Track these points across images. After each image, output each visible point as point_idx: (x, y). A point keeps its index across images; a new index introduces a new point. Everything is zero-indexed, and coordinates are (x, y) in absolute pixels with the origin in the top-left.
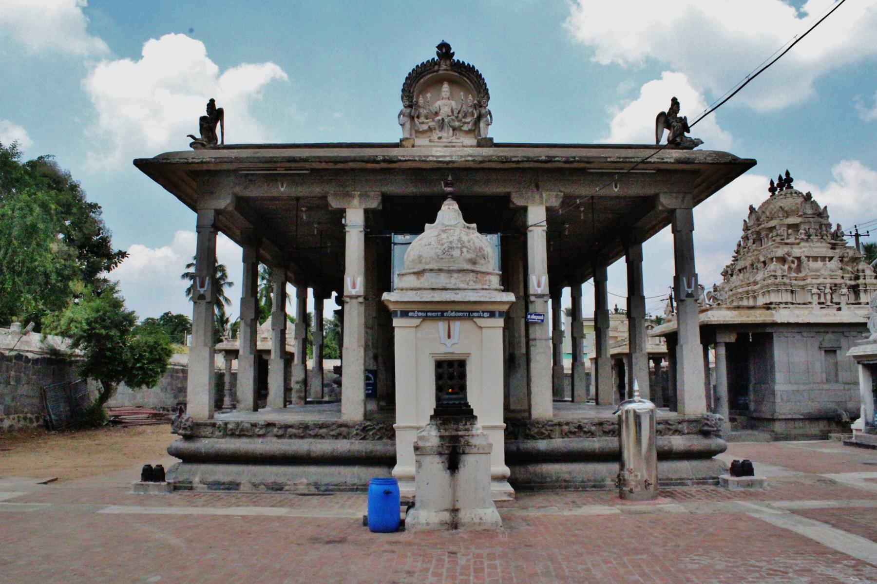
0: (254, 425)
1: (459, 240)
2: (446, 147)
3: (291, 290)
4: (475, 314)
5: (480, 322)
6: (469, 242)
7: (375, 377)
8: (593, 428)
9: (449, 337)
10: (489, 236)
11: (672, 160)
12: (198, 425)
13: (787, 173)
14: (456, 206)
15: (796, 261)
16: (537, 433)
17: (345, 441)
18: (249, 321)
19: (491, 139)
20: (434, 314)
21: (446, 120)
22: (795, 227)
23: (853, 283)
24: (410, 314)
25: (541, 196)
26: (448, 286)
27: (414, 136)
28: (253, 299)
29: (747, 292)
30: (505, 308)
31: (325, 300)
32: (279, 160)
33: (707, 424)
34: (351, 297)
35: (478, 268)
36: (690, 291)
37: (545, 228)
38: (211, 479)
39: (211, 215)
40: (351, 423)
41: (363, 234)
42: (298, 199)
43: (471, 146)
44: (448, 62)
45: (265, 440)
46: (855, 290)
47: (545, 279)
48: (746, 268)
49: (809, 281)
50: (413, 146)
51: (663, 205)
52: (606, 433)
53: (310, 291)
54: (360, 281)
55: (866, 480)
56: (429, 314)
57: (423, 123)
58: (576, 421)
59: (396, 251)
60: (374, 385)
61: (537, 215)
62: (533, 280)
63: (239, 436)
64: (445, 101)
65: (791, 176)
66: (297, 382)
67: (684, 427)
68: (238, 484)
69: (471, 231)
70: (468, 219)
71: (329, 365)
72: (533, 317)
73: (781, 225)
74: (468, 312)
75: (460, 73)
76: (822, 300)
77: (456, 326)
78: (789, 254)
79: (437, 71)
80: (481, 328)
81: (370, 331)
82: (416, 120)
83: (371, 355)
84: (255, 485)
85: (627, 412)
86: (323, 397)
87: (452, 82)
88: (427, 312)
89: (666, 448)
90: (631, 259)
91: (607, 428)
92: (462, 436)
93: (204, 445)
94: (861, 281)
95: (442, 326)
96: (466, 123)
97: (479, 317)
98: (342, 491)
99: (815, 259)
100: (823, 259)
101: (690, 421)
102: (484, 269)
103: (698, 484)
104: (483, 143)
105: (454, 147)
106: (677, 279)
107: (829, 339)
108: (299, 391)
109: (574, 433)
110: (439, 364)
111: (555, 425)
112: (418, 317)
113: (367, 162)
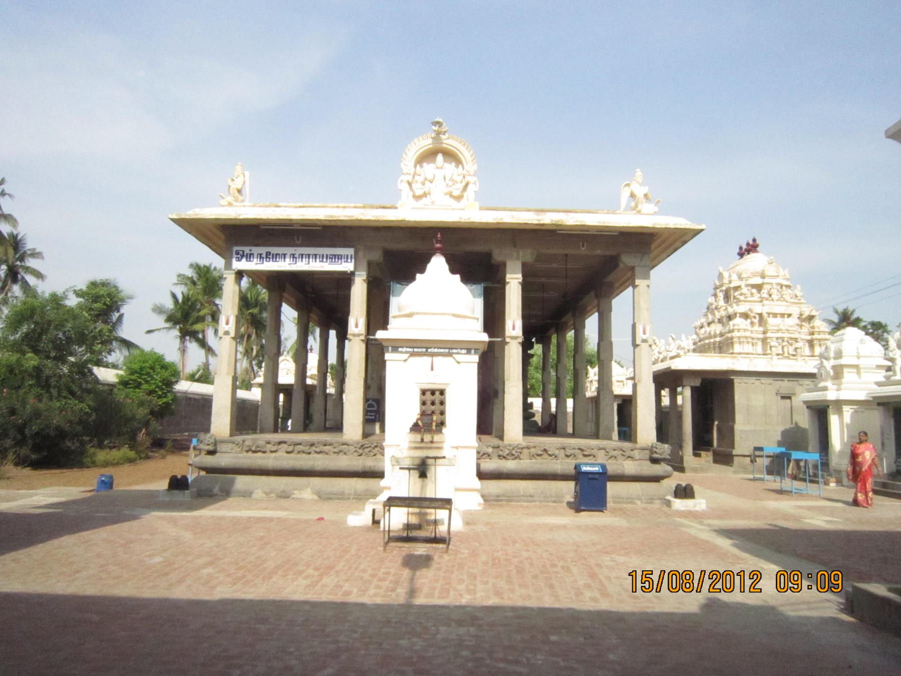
4: (454, 351)
8: (557, 452)
9: (432, 369)
10: (474, 287)
12: (222, 442)
13: (754, 240)
15: (757, 317)
17: (345, 456)
22: (759, 287)
23: (809, 338)
24: (400, 349)
28: (276, 337)
29: (714, 343)
33: (656, 452)
34: (354, 335)
36: (645, 337)
40: (351, 442)
46: (811, 343)
48: (713, 322)
49: (768, 335)
51: (624, 263)
52: (567, 456)
53: (333, 334)
55: (800, 507)
56: (416, 350)
62: (509, 324)
65: (758, 242)
67: (636, 454)
70: (453, 271)
73: (747, 285)
74: (449, 347)
76: (781, 352)
77: (438, 360)
78: (750, 310)
80: (459, 363)
94: (816, 336)
95: (427, 360)
97: (458, 353)
98: (339, 499)
99: (775, 315)
100: (782, 315)
101: (643, 449)
106: (634, 327)
107: (785, 385)
110: (424, 392)
112: (406, 352)
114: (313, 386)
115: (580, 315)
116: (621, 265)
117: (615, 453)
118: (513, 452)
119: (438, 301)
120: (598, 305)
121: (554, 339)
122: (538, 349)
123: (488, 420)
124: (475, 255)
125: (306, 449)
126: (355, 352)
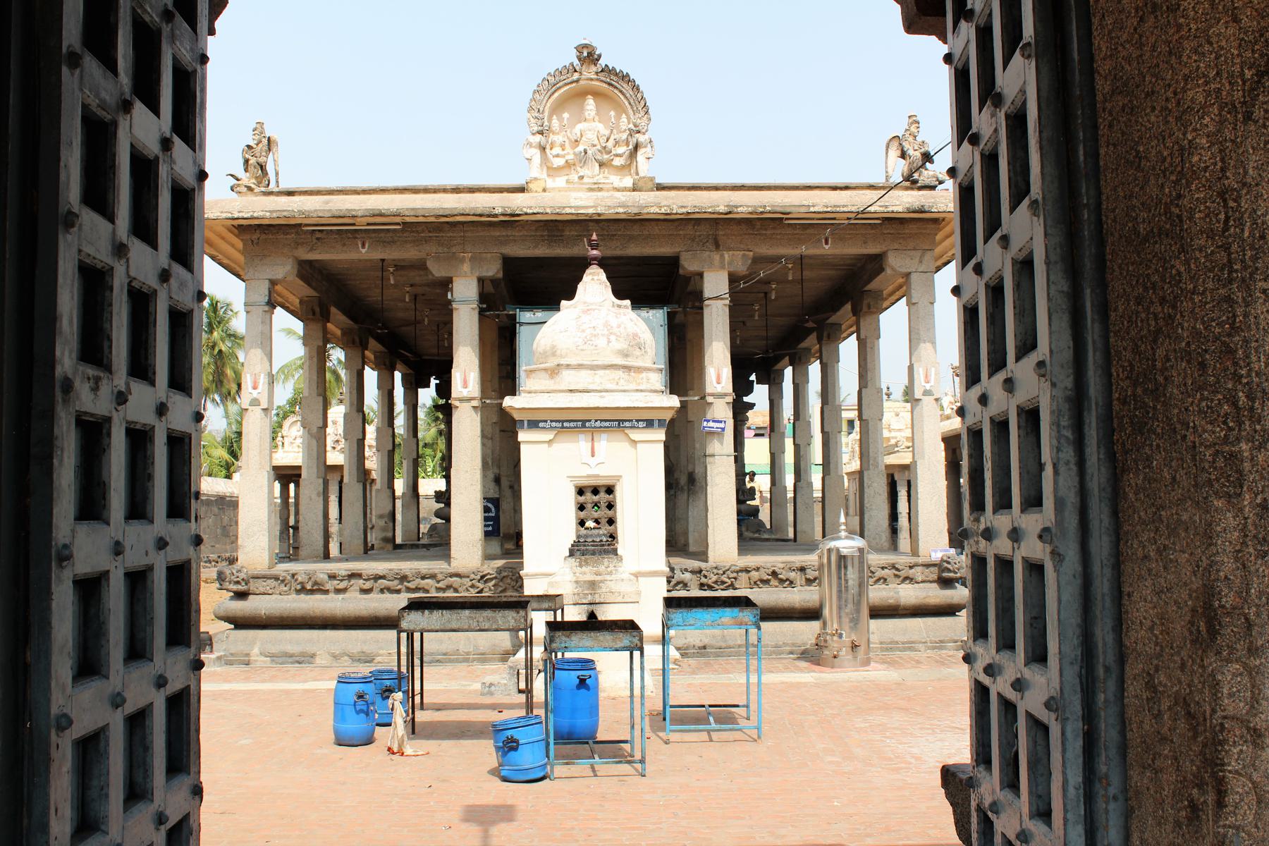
0: (332, 577)
1: (606, 324)
2: (591, 190)
3: (337, 355)
4: (627, 424)
5: (635, 435)
6: (619, 326)
7: (497, 507)
8: (792, 575)
10: (652, 312)
11: (900, 209)
14: (602, 275)
16: (716, 582)
18: (315, 430)
19: (652, 179)
20: (572, 424)
21: (589, 152)
24: (541, 425)
25: (722, 256)
26: (591, 387)
27: (544, 176)
30: (668, 416)
31: (420, 390)
32: (360, 214)
33: (949, 570)
34: (461, 400)
35: (630, 362)
37: (727, 302)
38: (274, 649)
39: (264, 288)
41: (477, 312)
42: (383, 260)
43: (625, 189)
44: (593, 69)
45: (347, 595)
47: (727, 372)
50: (544, 190)
51: (893, 269)
52: (809, 582)
53: (398, 376)
54: (474, 377)
57: (557, 156)
58: (769, 565)
59: (523, 333)
60: (496, 520)
61: (716, 285)
62: (711, 373)
63: (312, 592)
64: (592, 125)
66: (381, 517)
67: (918, 573)
68: (313, 656)
69: (622, 311)
70: (619, 293)
71: (430, 485)
72: (711, 424)
74: (619, 422)
75: (610, 84)
79: (577, 81)
80: (634, 442)
81: (489, 443)
82: (548, 151)
83: (491, 476)
84: (335, 657)
85: (829, 551)
86: (419, 539)
87: (596, 94)
88: (563, 421)
89: (891, 601)
90: (862, 336)
91: (811, 574)
92: (602, 581)
93: (256, 606)
96: (617, 155)
98: (450, 661)
101: (928, 566)
102: (640, 363)
103: (934, 648)
104: (640, 184)
105: (600, 190)
108: (384, 529)
109: (766, 582)
110: (580, 492)
111: (741, 571)
113: (481, 215)
114: (338, 468)
115: (830, 336)
116: (889, 271)
117: (880, 573)
118: (724, 578)
119: (594, 340)
120: (858, 324)
121: (788, 372)
122: (759, 395)
123: (679, 540)
124: (653, 272)
125: (394, 584)
126: (468, 429)
